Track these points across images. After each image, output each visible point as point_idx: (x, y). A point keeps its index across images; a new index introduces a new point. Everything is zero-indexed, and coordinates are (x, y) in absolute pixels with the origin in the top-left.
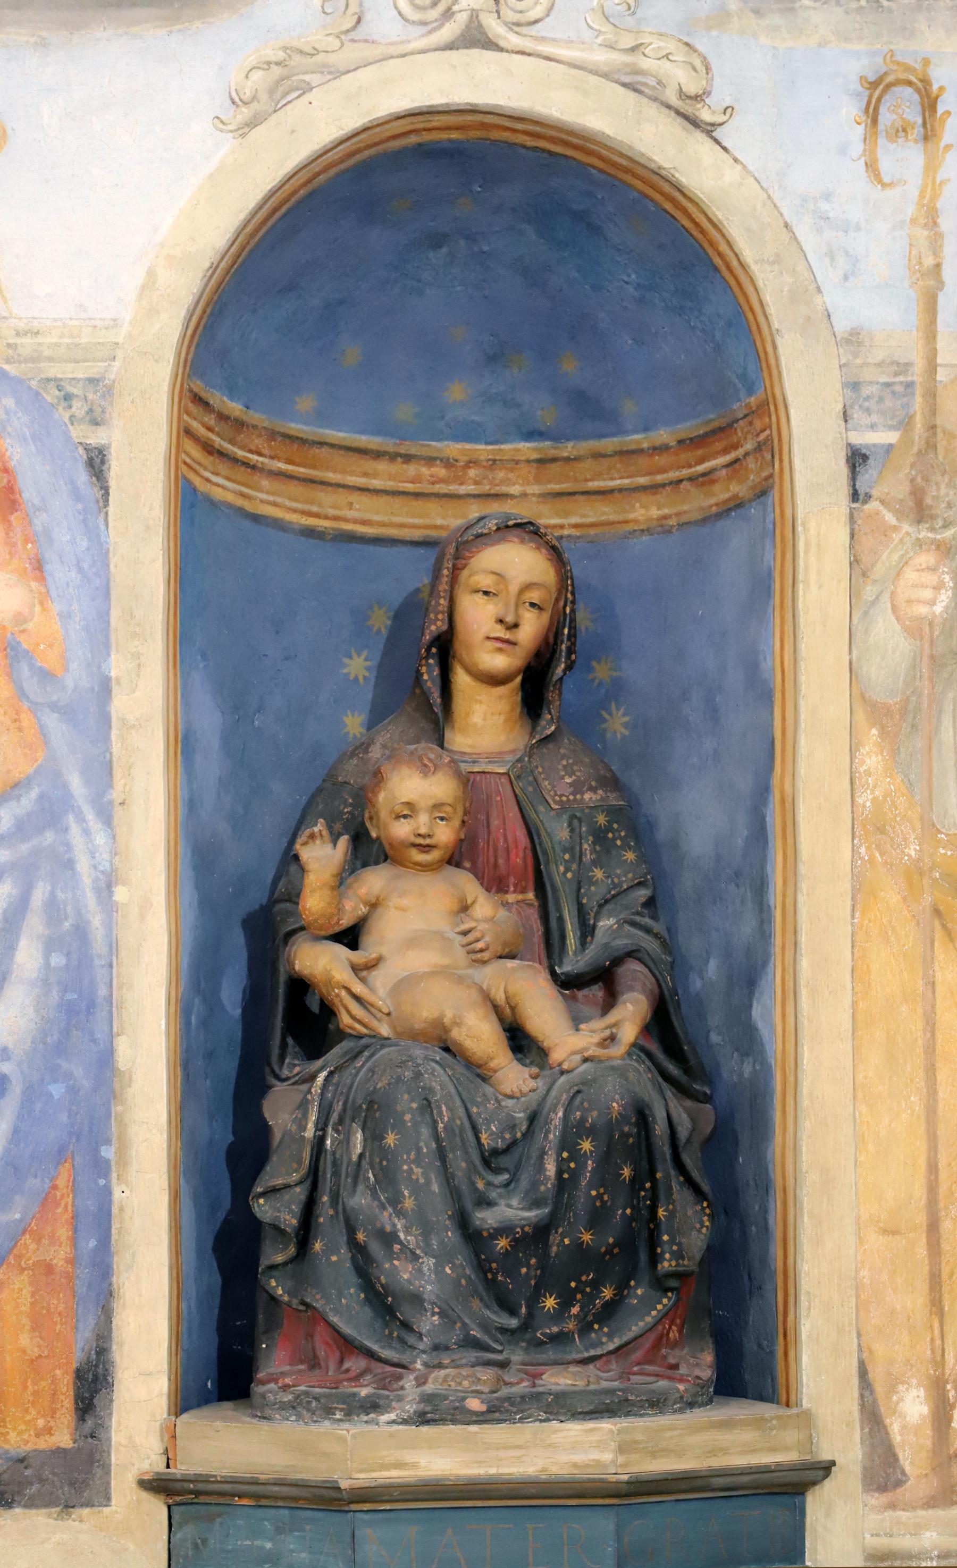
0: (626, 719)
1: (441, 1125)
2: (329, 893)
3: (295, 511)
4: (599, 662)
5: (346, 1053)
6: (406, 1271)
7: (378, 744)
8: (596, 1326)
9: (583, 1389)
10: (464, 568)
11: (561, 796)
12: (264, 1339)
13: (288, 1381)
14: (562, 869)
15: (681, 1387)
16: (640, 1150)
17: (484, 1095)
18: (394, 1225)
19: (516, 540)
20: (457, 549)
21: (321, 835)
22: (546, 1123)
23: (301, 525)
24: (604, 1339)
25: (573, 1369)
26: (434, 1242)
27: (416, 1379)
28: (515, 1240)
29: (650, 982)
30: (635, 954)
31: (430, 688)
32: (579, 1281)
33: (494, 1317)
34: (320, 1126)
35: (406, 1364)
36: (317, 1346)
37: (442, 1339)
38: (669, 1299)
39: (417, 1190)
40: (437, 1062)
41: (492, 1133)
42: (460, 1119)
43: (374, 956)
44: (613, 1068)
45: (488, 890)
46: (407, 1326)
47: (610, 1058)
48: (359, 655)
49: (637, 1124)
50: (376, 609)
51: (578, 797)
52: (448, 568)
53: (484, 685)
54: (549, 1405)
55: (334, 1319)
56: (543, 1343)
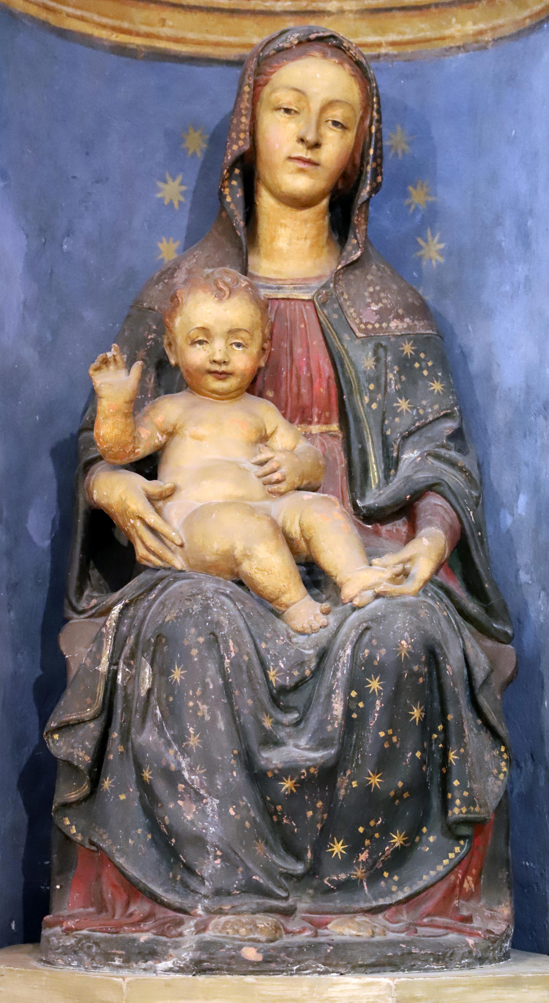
0: (442, 246)
1: (227, 661)
2: (124, 420)
3: (104, 26)
4: (415, 187)
5: (140, 587)
6: (189, 812)
7: (184, 269)
8: (386, 874)
9: (367, 940)
10: (266, 83)
11: (366, 324)
12: (57, 878)
13: (70, 924)
14: (367, 399)
15: (471, 941)
16: (431, 691)
17: (274, 631)
18: (179, 764)
19: (317, 54)
20: (259, 64)
21: (115, 360)
22: (336, 661)
23: (111, 41)
24: (394, 888)
25: (360, 918)
26: (218, 782)
27: (196, 926)
28: (300, 782)
29: (450, 516)
30: (435, 488)
31: (233, 211)
32: (367, 826)
33: (279, 862)
34: (114, 661)
35: (188, 909)
36: (104, 888)
37: (223, 883)
38: (462, 848)
39: (203, 728)
40: (227, 596)
41: (281, 670)
42: (248, 654)
43: (168, 485)
44: (404, 605)
45: (291, 421)
46: (189, 869)
47: (401, 595)
48: (174, 179)
49: (428, 663)
50: (191, 131)
51: (384, 325)
52: (249, 85)
53: (289, 208)
54: (328, 957)
55: (121, 860)
56: (333, 890)
